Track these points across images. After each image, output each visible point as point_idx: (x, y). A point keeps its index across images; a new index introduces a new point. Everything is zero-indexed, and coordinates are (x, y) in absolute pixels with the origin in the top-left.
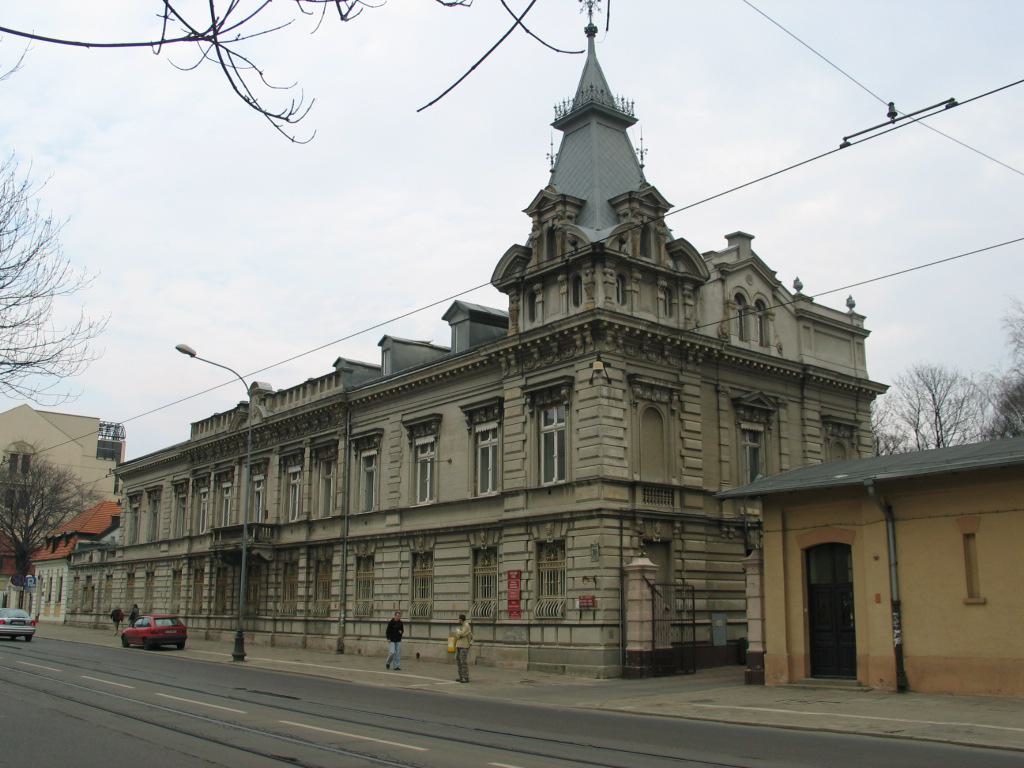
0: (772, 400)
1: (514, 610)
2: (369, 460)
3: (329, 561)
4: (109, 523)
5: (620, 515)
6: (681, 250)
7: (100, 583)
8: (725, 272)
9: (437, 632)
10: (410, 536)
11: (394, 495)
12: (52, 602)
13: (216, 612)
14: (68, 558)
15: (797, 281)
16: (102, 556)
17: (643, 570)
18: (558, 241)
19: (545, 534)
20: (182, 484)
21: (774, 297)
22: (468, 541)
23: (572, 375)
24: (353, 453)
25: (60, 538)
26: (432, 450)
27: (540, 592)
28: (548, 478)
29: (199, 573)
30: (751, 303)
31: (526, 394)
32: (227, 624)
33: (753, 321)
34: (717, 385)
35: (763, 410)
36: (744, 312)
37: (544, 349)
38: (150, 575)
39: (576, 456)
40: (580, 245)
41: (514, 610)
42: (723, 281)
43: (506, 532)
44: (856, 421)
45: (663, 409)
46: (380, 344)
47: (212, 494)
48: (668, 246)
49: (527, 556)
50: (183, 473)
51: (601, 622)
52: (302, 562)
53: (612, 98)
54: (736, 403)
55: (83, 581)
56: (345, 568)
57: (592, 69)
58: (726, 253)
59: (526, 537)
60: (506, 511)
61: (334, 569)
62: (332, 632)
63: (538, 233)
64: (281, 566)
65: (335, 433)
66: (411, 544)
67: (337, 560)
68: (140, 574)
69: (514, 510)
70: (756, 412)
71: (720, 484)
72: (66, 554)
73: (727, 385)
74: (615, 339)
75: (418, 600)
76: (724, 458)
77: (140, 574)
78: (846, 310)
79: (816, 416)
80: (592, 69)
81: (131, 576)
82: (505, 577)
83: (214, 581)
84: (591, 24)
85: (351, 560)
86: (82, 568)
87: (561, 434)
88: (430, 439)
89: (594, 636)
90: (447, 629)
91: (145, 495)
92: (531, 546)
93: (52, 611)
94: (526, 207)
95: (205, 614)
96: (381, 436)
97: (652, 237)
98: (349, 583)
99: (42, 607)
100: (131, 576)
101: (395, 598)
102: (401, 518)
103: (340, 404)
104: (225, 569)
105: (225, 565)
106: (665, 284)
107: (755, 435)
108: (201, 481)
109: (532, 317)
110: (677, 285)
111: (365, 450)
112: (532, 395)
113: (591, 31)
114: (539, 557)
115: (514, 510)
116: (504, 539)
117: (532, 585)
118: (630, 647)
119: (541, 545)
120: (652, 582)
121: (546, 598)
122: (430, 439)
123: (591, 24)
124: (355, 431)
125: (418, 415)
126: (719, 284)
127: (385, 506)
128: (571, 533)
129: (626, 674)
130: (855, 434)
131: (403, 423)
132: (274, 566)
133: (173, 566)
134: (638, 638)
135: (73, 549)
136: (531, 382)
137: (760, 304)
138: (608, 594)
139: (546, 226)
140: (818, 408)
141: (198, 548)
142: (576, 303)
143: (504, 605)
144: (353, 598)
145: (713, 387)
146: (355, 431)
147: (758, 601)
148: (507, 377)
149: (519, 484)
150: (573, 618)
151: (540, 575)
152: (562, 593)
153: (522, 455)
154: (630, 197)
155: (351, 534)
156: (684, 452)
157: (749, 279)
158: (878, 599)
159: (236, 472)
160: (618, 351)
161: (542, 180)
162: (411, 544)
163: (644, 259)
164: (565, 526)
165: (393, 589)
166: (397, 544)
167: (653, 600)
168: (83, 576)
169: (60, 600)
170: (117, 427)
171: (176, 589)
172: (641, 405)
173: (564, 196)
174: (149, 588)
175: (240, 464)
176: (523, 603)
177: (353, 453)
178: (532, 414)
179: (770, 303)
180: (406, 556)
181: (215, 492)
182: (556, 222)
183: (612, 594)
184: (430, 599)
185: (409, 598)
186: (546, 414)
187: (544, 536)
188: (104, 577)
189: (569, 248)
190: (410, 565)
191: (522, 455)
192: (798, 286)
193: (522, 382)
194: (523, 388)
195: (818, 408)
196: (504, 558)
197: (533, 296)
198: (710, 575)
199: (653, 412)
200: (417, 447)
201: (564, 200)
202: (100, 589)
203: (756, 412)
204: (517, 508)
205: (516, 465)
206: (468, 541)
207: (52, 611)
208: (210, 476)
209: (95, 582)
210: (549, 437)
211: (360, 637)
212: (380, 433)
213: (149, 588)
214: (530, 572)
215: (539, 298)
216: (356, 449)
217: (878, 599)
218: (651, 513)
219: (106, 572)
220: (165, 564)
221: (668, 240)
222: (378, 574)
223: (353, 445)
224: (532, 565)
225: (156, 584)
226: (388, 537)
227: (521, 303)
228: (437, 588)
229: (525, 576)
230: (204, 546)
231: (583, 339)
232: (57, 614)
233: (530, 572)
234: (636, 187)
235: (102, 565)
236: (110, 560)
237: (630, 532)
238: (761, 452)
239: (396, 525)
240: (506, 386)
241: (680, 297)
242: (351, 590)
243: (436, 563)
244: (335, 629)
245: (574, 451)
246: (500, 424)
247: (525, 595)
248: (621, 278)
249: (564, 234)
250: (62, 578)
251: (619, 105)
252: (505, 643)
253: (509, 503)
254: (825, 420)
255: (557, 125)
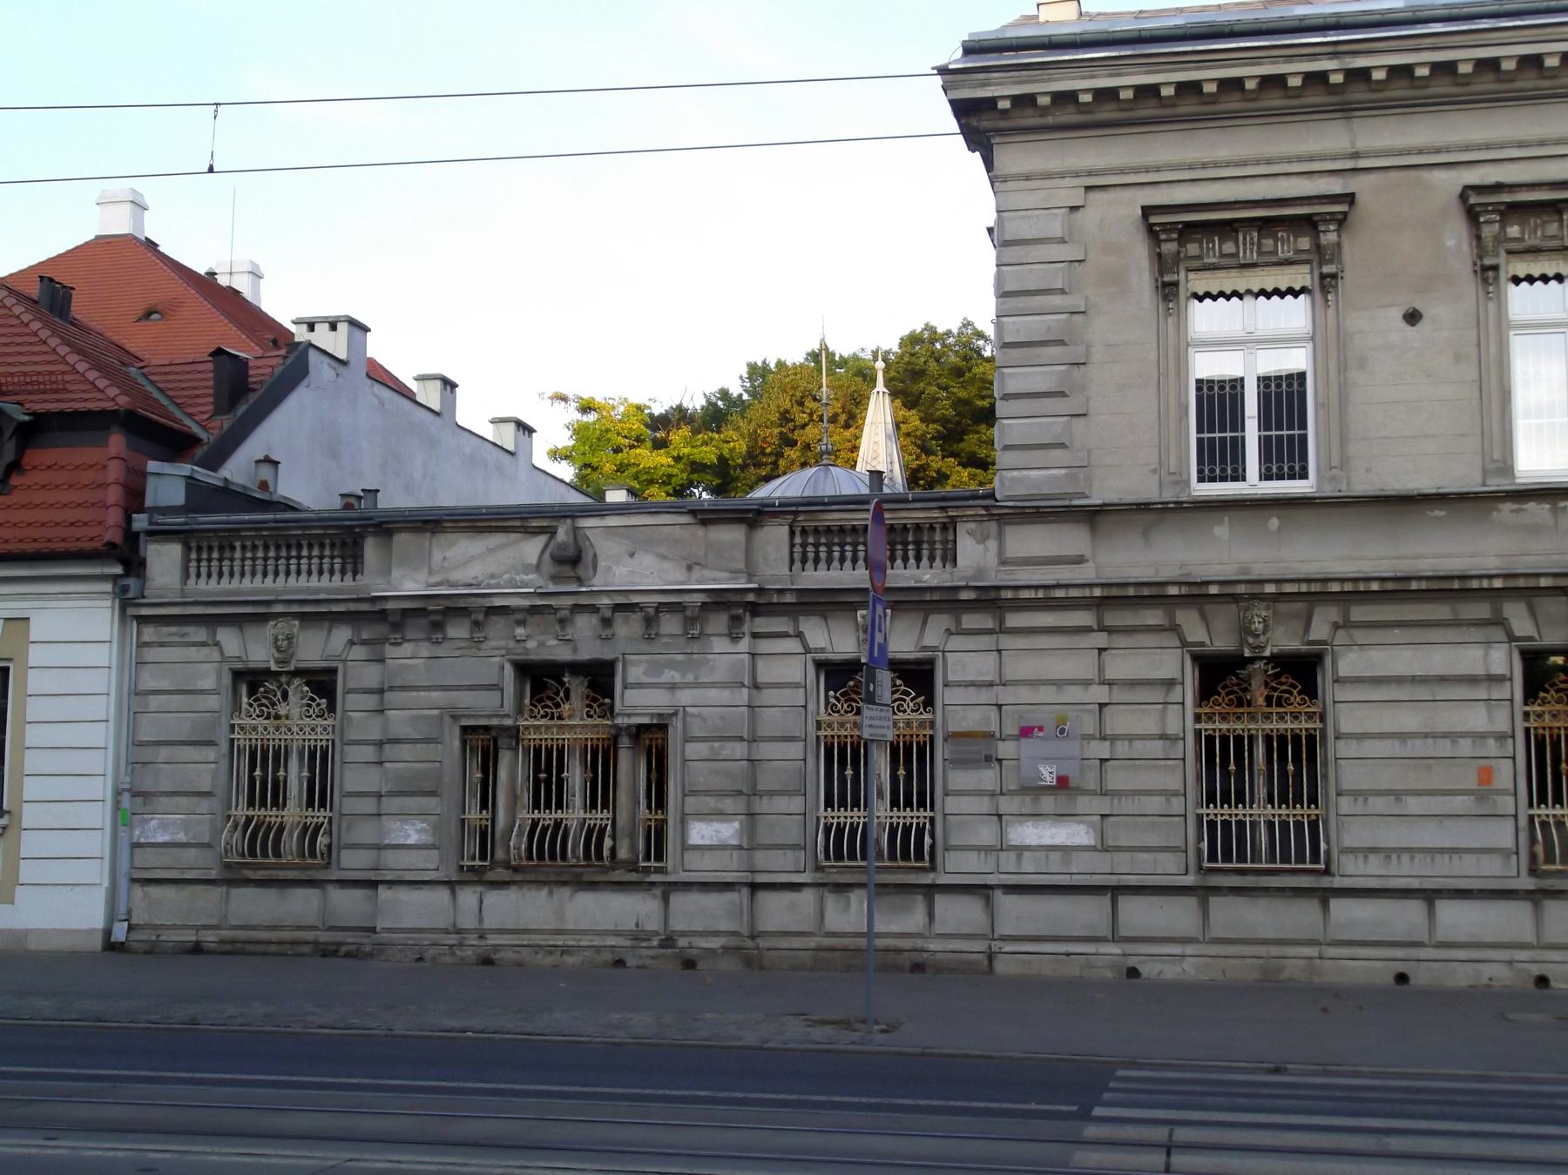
128: (956, 642)
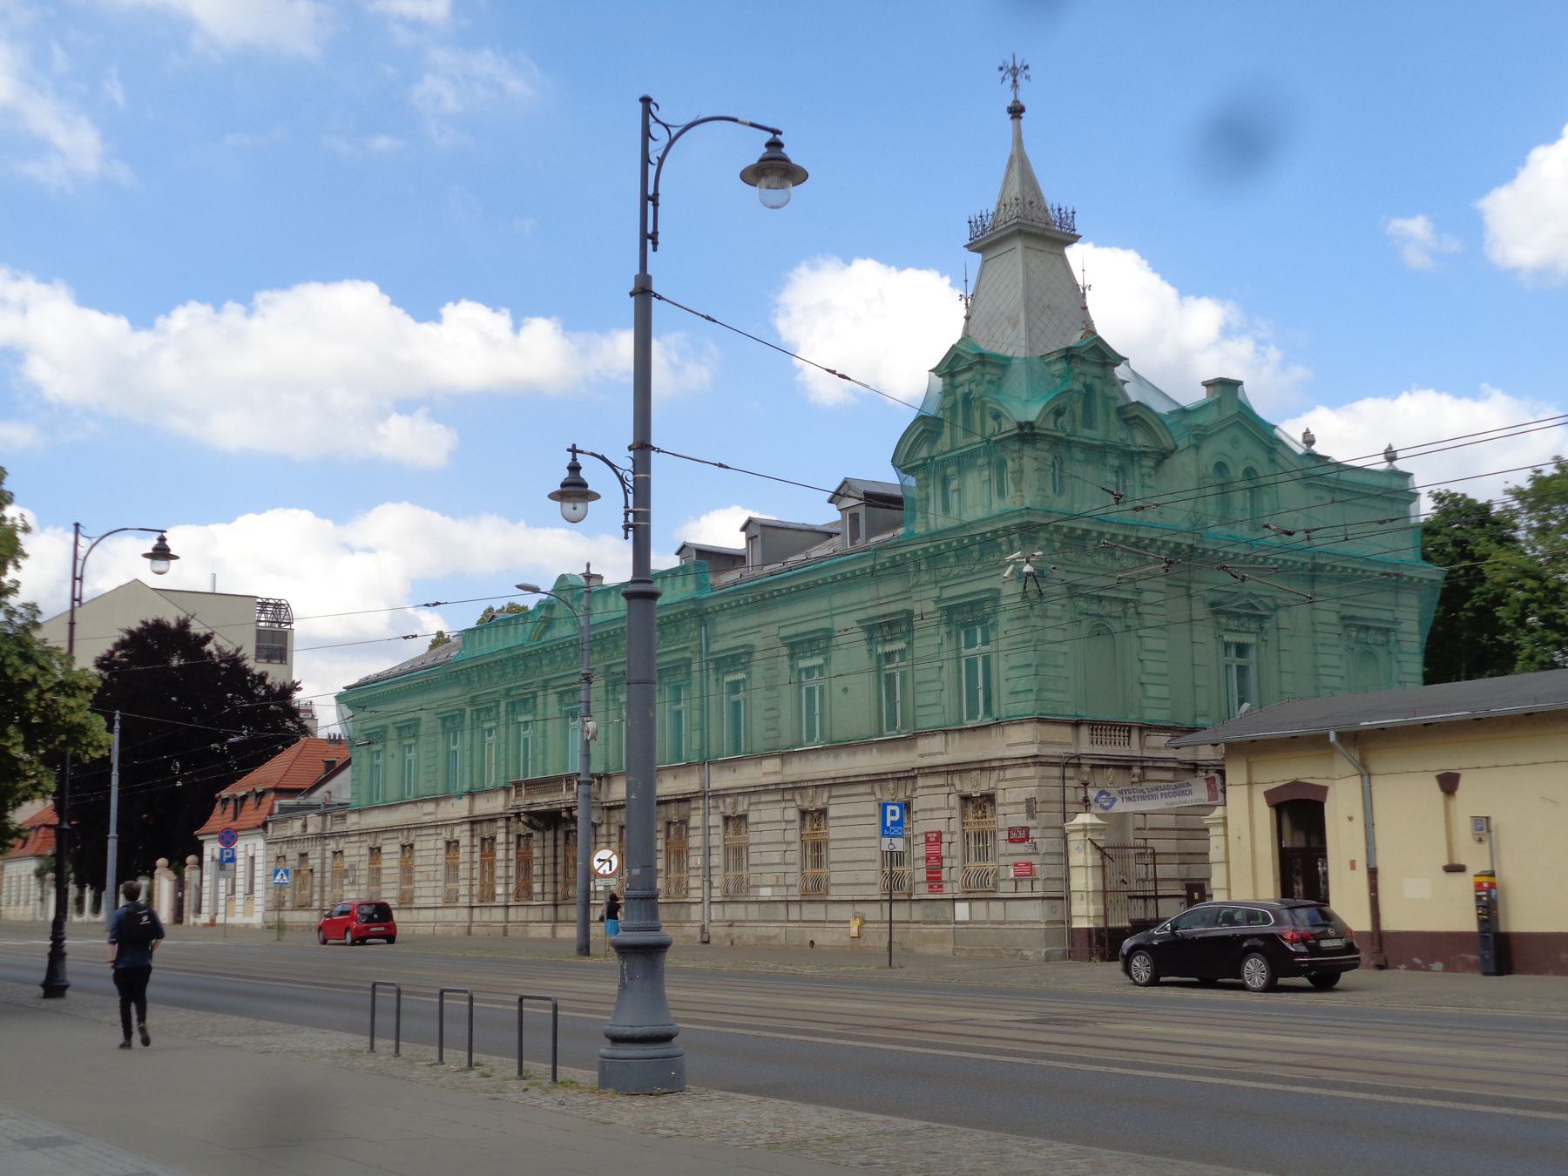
0: (1266, 600)
1: (934, 878)
2: (735, 687)
3: (684, 822)
4: (320, 771)
5: (1037, 761)
6: (1137, 417)
7: (323, 863)
8: (1200, 437)
9: (837, 912)
10: (798, 787)
11: (771, 734)
12: (239, 895)
13: (518, 897)
14: (265, 825)
15: (1307, 433)
16: (324, 823)
17: (1085, 829)
18: (977, 414)
19: (975, 785)
20: (453, 717)
21: (1272, 461)
22: (873, 793)
23: (1000, 586)
24: (712, 677)
25: (244, 798)
26: (821, 674)
27: (966, 858)
28: (972, 714)
29: (488, 843)
30: (1237, 472)
31: (942, 609)
32: (534, 914)
33: (1239, 499)
34: (1188, 588)
35: (1254, 616)
36: (1225, 489)
37: (961, 551)
38: (407, 848)
39: (1005, 688)
40: (1003, 421)
41: (934, 878)
42: (1197, 448)
43: (921, 782)
44: (1396, 621)
45: (1116, 626)
46: (744, 529)
47: (502, 730)
48: (1121, 411)
49: (947, 814)
50: (453, 697)
51: (1040, 895)
52: (501, 838)
53: (1046, 211)
54: (1216, 609)
55: (293, 861)
56: (707, 830)
57: (1020, 162)
58: (1201, 408)
59: (947, 790)
60: (922, 756)
61: (691, 833)
62: (693, 917)
63: (948, 403)
64: (614, 830)
65: (685, 649)
66: (798, 798)
67: (695, 820)
68: (391, 847)
69: (930, 754)
70: (1243, 616)
71: (1195, 716)
72: (260, 822)
73: (1204, 587)
74: (1050, 541)
75: (809, 871)
76: (1197, 682)
77: (391, 847)
78: (1384, 466)
79: (1333, 618)
80: (1020, 162)
81: (375, 851)
82: (922, 839)
83: (512, 854)
84: (1016, 101)
85: (716, 819)
86: (290, 841)
87: (986, 660)
88: (818, 661)
89: (1034, 913)
90: (849, 907)
91: (392, 733)
92: (954, 801)
93: (239, 909)
94: (934, 365)
95: (500, 900)
96: (750, 654)
97: (1099, 402)
98: (713, 851)
99: (222, 903)
100: (375, 851)
101: (777, 869)
102: (783, 762)
103: (692, 611)
104: (530, 835)
105: (529, 831)
106: (1116, 463)
107: (1242, 649)
108: (483, 710)
109: (946, 508)
110: (1132, 461)
111: (728, 673)
112: (949, 611)
113: (1016, 111)
114: (964, 814)
115: (930, 754)
116: (919, 792)
117: (957, 849)
118: (1078, 924)
119: (966, 799)
120: (1101, 845)
121: (973, 865)
122: (818, 661)
123: (1016, 101)
124: (714, 647)
125: (802, 628)
126: (1192, 453)
127: (759, 746)
128: (1002, 785)
129: (1070, 955)
130: (1393, 638)
131: (782, 639)
132: (603, 830)
133: (370, 842)
134: (1085, 914)
135: (270, 814)
136: (947, 594)
137: (1250, 473)
138: (1048, 859)
139: (959, 391)
140: (1337, 607)
141: (484, 806)
142: (1001, 493)
143: (921, 875)
144: (721, 871)
145: (1183, 591)
146: (714, 647)
147: (1223, 866)
148: (915, 586)
149: (935, 722)
150: (1006, 889)
151: (966, 837)
152: (994, 859)
153: (938, 686)
154: (1069, 355)
155: (715, 785)
156: (1144, 679)
157: (1235, 442)
158: (1353, 865)
159: (540, 700)
160: (1054, 557)
161: (955, 336)
162: (798, 798)
163: (1087, 432)
164: (995, 775)
165: (776, 858)
166: (779, 797)
167: (1103, 866)
168: (292, 854)
169: (233, 892)
170: (278, 605)
171: (452, 869)
172: (1086, 622)
173: (982, 355)
174: (407, 870)
175: (545, 688)
176: (945, 872)
177: (712, 677)
178: (949, 633)
179: (1263, 468)
180: (792, 814)
181: (507, 725)
182: (973, 386)
183: (1055, 860)
184: (824, 870)
185: (796, 868)
186: (967, 633)
187: (968, 789)
188: (329, 854)
189: (991, 424)
190: (797, 825)
191: (938, 686)
192: (1309, 440)
193: (935, 593)
194: (938, 600)
195: (1337, 607)
196: (920, 816)
197: (945, 481)
198: (1183, 834)
199: (1100, 630)
200: (800, 670)
201: (983, 359)
202: (323, 872)
203: (1243, 616)
204: (934, 751)
205: (931, 699)
206: (873, 793)
207: (239, 909)
208: (498, 706)
209: (314, 861)
210: (971, 663)
211: (731, 924)
212: (749, 651)
213: (407, 870)
214: (953, 833)
215: (954, 485)
216: (717, 669)
217: (1353, 865)
218: (1100, 757)
219: (370, 842)
220: (432, 831)
221: (1121, 403)
222: (754, 838)
223: (712, 666)
224: (955, 825)
225: (418, 861)
226: (765, 789)
227: (931, 490)
228: (833, 855)
229: (946, 838)
230: (495, 804)
231: (1011, 542)
232: (248, 912)
233: (953, 833)
234: (1075, 339)
235: (322, 837)
236: (336, 829)
237: (1075, 783)
238: (1252, 670)
239: (776, 773)
240: (916, 597)
241: (1138, 478)
242: (717, 859)
243: (831, 823)
244: (696, 913)
245: (1002, 682)
246: (910, 643)
247: (946, 863)
248: (1058, 463)
249: (984, 403)
250: (253, 858)
251: (1054, 215)
252: (925, 923)
253: (924, 745)
254: (1347, 621)
255: (972, 247)
